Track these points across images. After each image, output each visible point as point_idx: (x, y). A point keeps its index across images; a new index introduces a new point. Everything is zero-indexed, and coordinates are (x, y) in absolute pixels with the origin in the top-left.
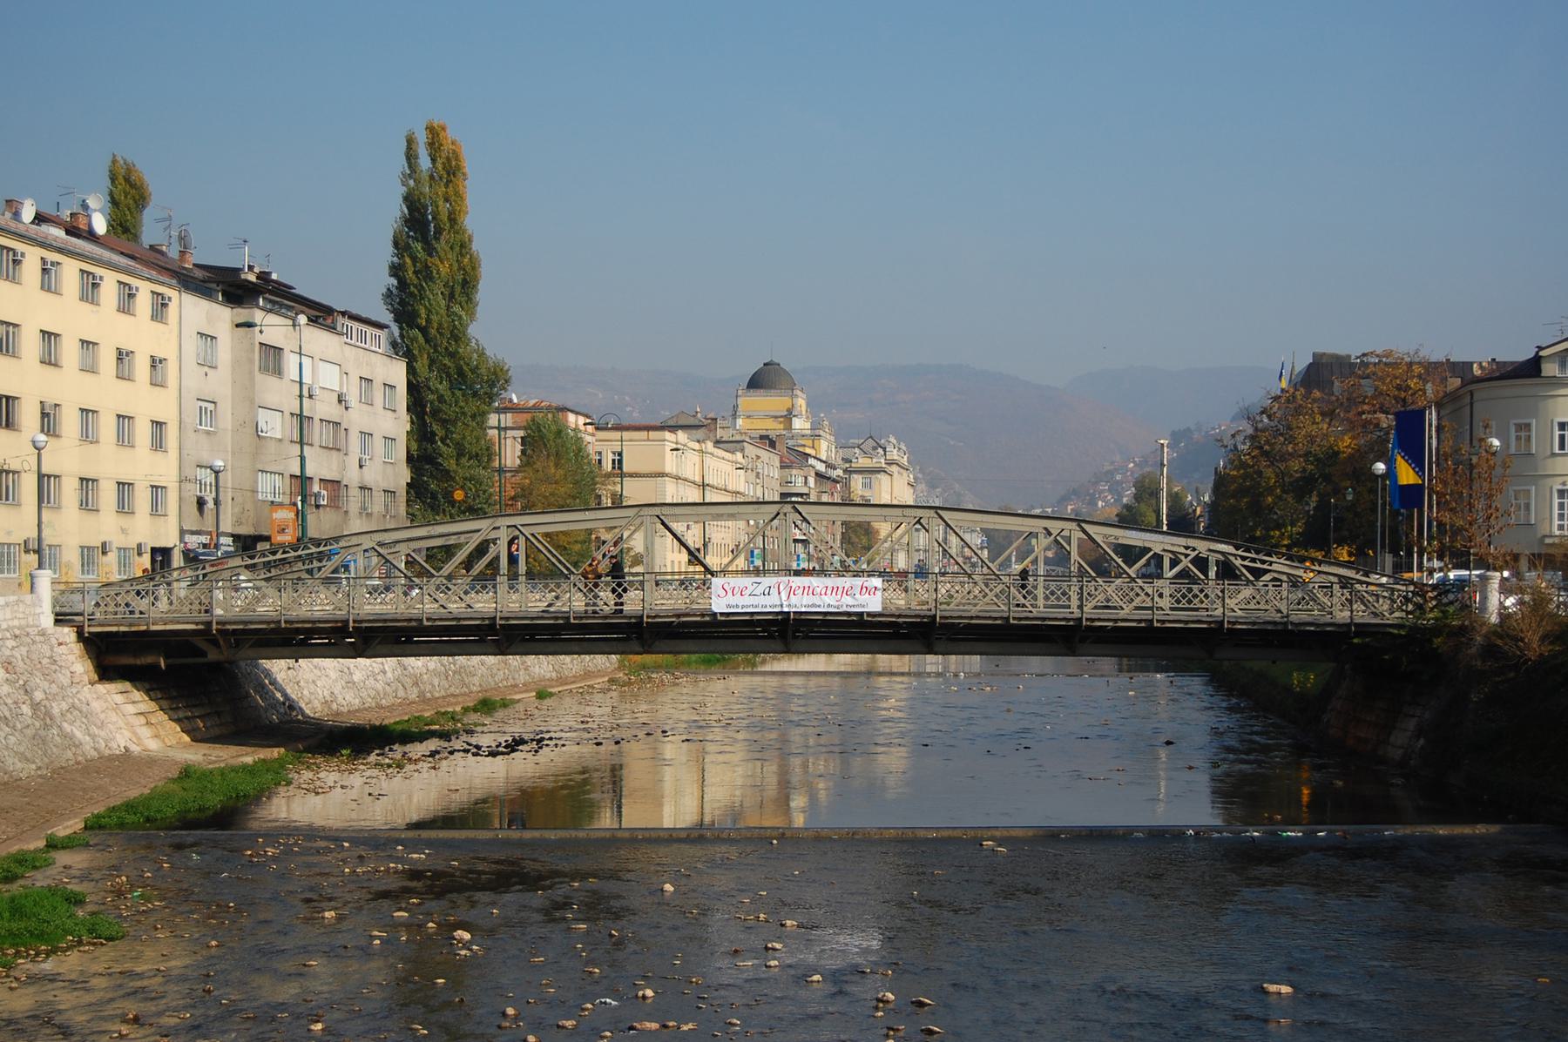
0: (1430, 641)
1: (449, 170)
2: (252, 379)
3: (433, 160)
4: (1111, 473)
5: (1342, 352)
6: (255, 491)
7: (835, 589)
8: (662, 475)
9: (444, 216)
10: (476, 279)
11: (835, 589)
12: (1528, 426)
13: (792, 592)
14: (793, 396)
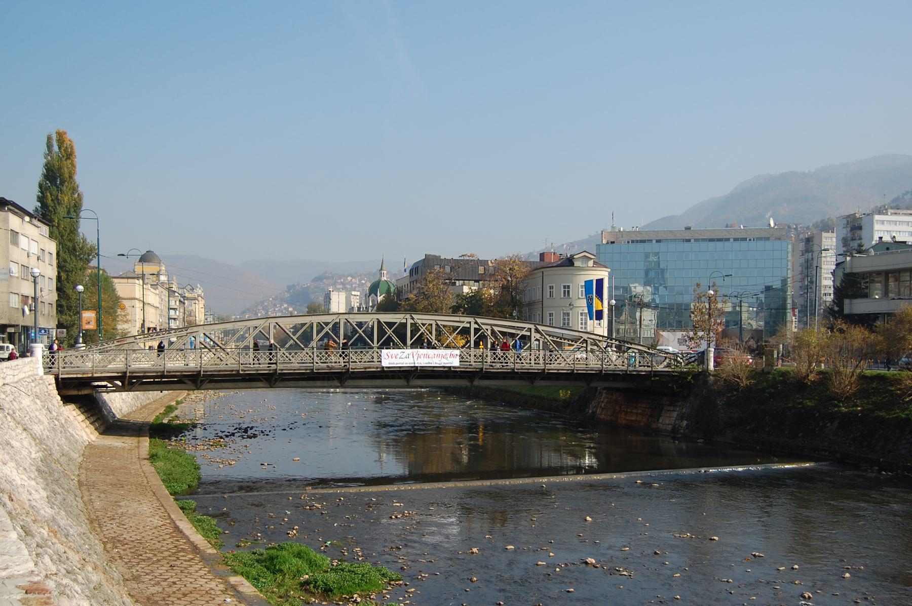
0: (686, 378)
1: (69, 155)
2: (8, 248)
3: (60, 148)
4: (263, 302)
5: (437, 254)
6: (9, 302)
7: (438, 356)
8: (135, 299)
9: (67, 175)
10: (81, 205)
11: (438, 356)
12: (569, 287)
13: (419, 357)
14: (160, 266)
